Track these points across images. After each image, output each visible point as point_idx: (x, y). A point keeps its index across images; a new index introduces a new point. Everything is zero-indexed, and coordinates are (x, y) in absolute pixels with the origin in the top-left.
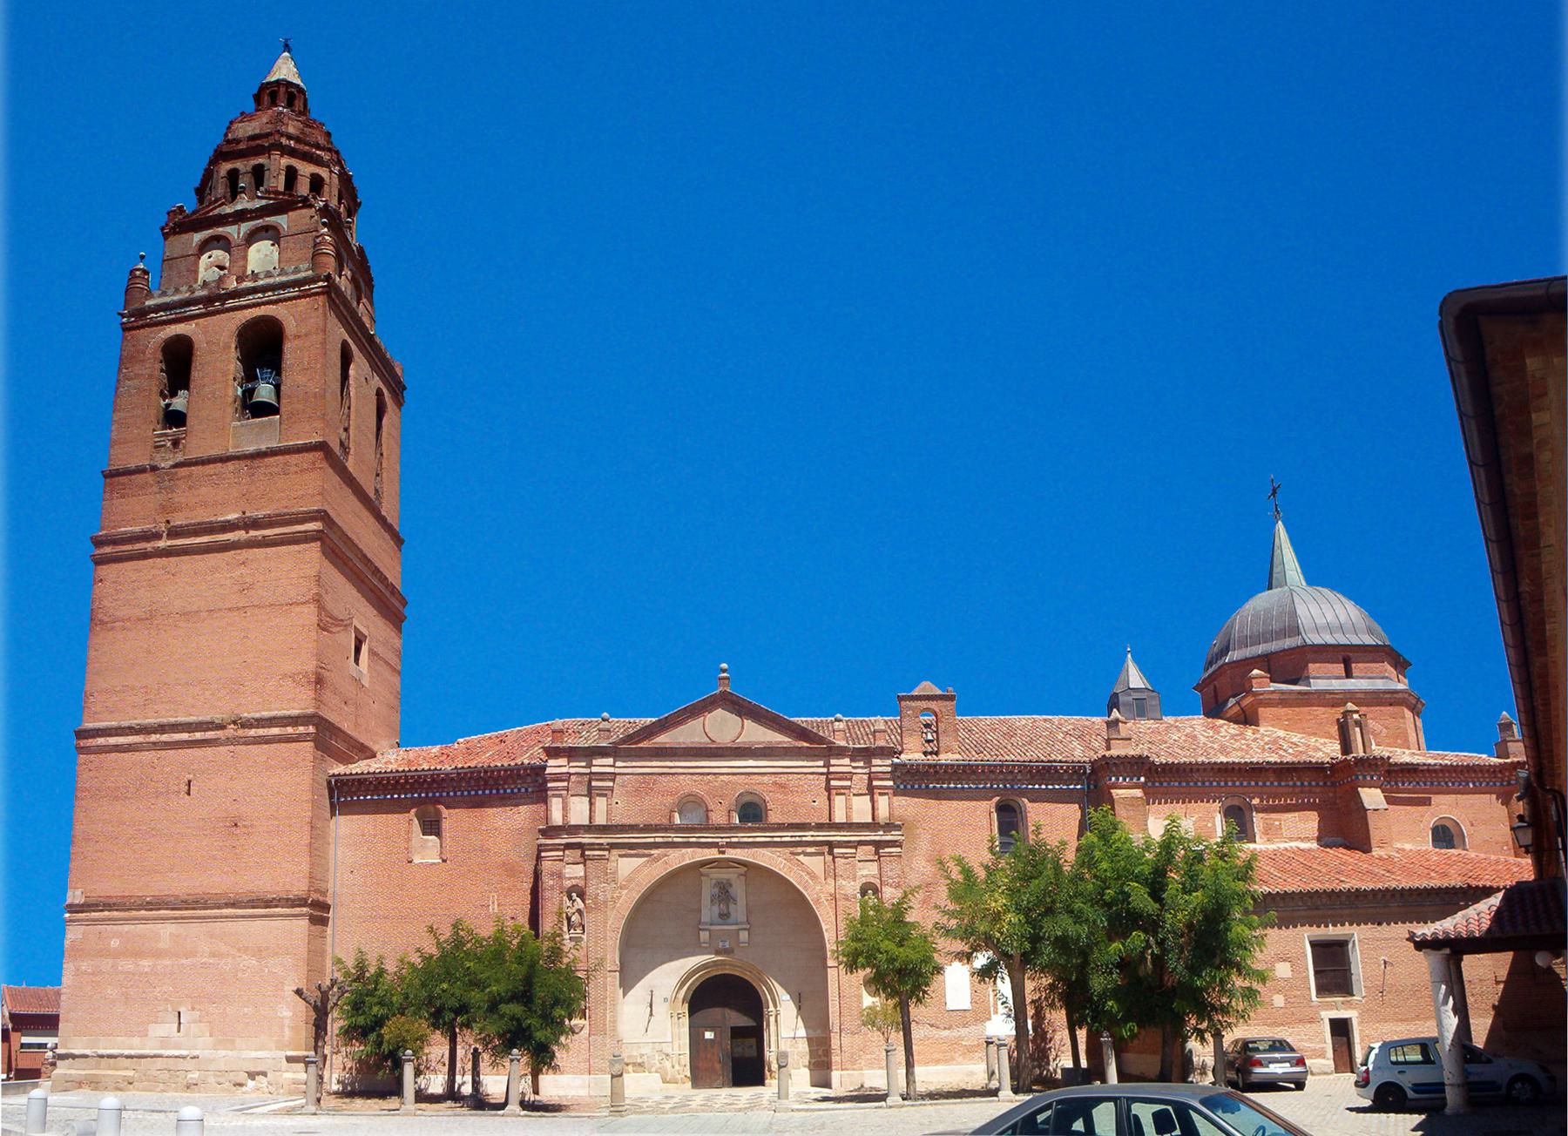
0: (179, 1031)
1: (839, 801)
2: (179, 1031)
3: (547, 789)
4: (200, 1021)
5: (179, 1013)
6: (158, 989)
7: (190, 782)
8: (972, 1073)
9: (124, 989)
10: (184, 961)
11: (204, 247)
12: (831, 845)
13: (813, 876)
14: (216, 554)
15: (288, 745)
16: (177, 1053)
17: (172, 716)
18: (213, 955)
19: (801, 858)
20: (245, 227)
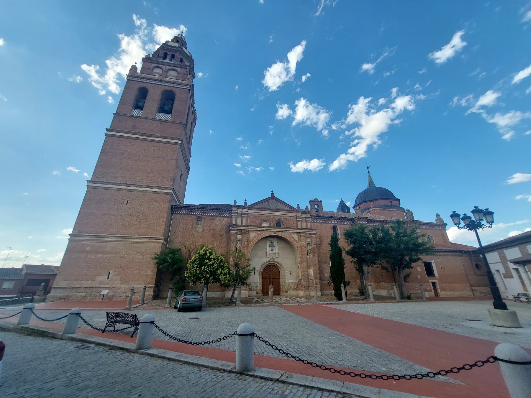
0: (108, 279)
1: (299, 223)
2: (108, 279)
3: (232, 216)
4: (117, 275)
5: (110, 272)
6: (103, 264)
7: (128, 201)
8: (332, 293)
9: (89, 264)
10: (115, 255)
11: (155, 67)
12: (300, 233)
13: (296, 241)
14: (396, 392)
15: (163, 195)
16: (106, 286)
17: (125, 182)
18: (126, 254)
19: (293, 236)
20: (168, 67)
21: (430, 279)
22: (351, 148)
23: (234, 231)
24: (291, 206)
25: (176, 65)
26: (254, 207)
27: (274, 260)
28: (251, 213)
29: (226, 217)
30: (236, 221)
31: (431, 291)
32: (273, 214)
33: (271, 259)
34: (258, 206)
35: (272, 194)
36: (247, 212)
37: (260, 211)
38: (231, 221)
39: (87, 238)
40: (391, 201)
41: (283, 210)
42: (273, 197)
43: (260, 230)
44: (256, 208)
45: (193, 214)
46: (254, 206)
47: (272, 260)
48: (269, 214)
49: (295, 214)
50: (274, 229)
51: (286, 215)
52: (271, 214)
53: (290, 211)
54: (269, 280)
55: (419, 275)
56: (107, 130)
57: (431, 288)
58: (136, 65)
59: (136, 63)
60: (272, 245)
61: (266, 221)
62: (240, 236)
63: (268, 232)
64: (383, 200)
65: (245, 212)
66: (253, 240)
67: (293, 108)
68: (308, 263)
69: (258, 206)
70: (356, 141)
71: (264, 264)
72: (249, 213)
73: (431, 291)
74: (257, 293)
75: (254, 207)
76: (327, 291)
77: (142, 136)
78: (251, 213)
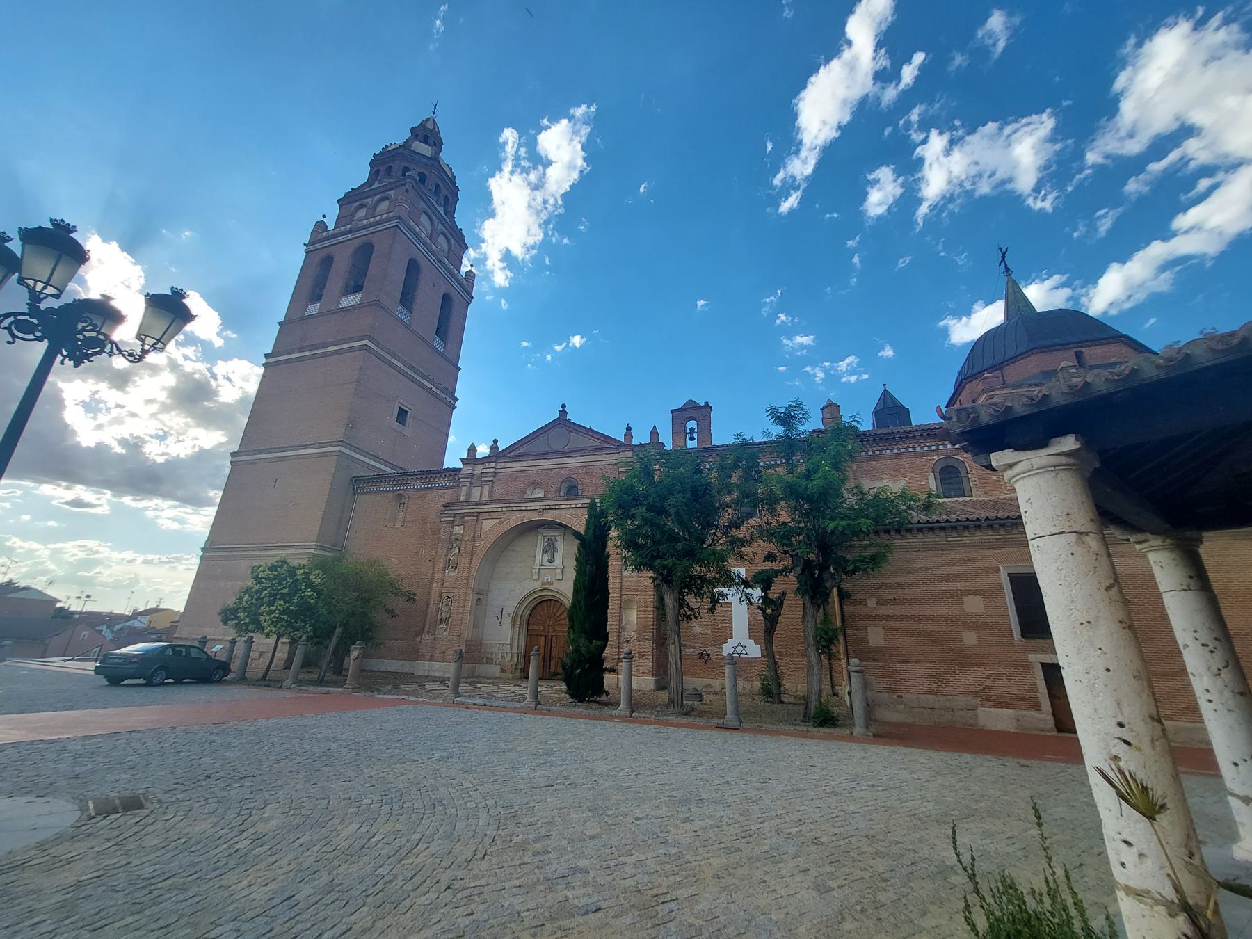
21: (1035, 652)
22: (1185, 209)
23: (446, 519)
24: (605, 436)
25: (388, 188)
26: (511, 454)
27: (550, 587)
28: (503, 470)
29: (450, 487)
30: (469, 494)
31: (1036, 706)
32: (556, 466)
33: (543, 584)
34: (521, 450)
35: (563, 412)
36: (493, 470)
37: (525, 463)
38: (459, 496)
39: (258, 553)
40: (1079, 356)
41: (581, 451)
42: (562, 420)
43: (504, 509)
44: (519, 456)
45: (389, 491)
46: (517, 451)
47: (547, 587)
48: (546, 467)
49: (615, 456)
50: (566, 502)
51: (590, 464)
52: (551, 467)
53: (602, 449)
54: (543, 638)
55: (968, 629)
56: (267, 356)
57: (1034, 688)
58: (325, 220)
59: (324, 216)
60: (551, 548)
61: (536, 485)
62: (459, 530)
63: (525, 513)
64: (1036, 358)
65: (488, 470)
66: (487, 536)
67: (910, 167)
68: (623, 593)
69: (521, 450)
70: (1204, 184)
71: (525, 598)
72: (497, 471)
73: (1036, 706)
74: (503, 671)
75: (511, 454)
76: (695, 679)
77: (311, 350)
78: (503, 470)
